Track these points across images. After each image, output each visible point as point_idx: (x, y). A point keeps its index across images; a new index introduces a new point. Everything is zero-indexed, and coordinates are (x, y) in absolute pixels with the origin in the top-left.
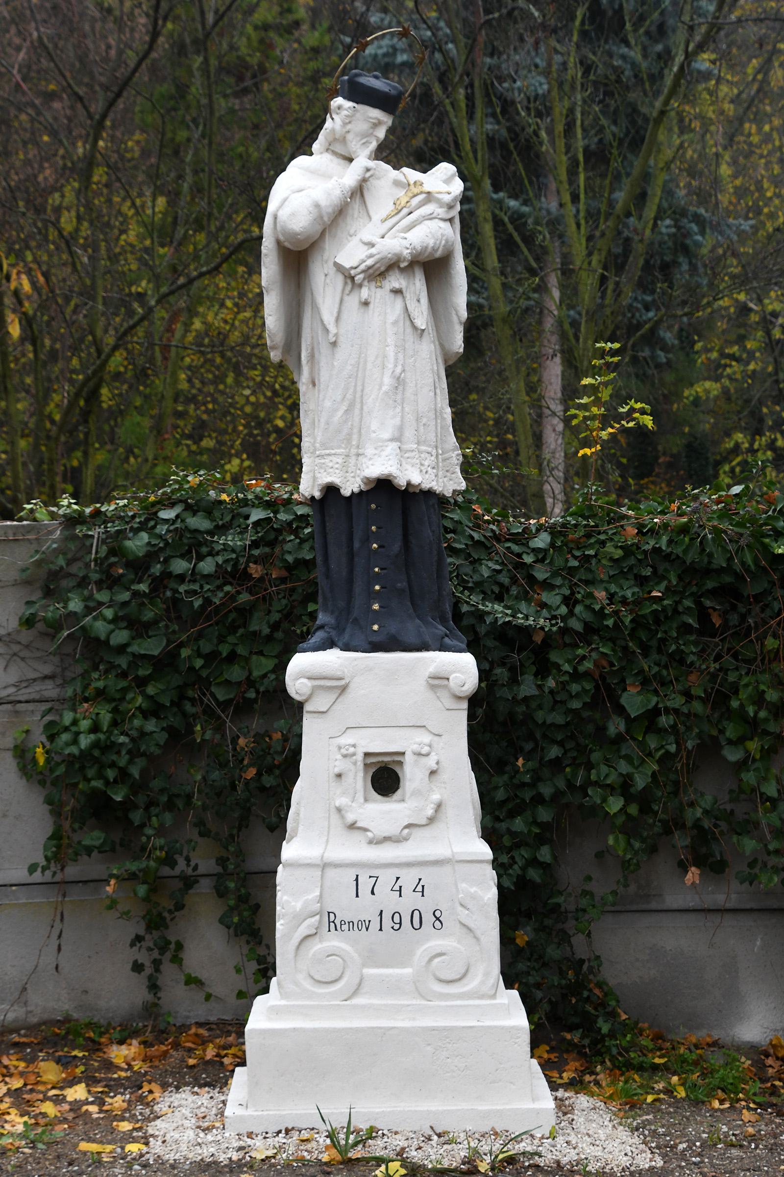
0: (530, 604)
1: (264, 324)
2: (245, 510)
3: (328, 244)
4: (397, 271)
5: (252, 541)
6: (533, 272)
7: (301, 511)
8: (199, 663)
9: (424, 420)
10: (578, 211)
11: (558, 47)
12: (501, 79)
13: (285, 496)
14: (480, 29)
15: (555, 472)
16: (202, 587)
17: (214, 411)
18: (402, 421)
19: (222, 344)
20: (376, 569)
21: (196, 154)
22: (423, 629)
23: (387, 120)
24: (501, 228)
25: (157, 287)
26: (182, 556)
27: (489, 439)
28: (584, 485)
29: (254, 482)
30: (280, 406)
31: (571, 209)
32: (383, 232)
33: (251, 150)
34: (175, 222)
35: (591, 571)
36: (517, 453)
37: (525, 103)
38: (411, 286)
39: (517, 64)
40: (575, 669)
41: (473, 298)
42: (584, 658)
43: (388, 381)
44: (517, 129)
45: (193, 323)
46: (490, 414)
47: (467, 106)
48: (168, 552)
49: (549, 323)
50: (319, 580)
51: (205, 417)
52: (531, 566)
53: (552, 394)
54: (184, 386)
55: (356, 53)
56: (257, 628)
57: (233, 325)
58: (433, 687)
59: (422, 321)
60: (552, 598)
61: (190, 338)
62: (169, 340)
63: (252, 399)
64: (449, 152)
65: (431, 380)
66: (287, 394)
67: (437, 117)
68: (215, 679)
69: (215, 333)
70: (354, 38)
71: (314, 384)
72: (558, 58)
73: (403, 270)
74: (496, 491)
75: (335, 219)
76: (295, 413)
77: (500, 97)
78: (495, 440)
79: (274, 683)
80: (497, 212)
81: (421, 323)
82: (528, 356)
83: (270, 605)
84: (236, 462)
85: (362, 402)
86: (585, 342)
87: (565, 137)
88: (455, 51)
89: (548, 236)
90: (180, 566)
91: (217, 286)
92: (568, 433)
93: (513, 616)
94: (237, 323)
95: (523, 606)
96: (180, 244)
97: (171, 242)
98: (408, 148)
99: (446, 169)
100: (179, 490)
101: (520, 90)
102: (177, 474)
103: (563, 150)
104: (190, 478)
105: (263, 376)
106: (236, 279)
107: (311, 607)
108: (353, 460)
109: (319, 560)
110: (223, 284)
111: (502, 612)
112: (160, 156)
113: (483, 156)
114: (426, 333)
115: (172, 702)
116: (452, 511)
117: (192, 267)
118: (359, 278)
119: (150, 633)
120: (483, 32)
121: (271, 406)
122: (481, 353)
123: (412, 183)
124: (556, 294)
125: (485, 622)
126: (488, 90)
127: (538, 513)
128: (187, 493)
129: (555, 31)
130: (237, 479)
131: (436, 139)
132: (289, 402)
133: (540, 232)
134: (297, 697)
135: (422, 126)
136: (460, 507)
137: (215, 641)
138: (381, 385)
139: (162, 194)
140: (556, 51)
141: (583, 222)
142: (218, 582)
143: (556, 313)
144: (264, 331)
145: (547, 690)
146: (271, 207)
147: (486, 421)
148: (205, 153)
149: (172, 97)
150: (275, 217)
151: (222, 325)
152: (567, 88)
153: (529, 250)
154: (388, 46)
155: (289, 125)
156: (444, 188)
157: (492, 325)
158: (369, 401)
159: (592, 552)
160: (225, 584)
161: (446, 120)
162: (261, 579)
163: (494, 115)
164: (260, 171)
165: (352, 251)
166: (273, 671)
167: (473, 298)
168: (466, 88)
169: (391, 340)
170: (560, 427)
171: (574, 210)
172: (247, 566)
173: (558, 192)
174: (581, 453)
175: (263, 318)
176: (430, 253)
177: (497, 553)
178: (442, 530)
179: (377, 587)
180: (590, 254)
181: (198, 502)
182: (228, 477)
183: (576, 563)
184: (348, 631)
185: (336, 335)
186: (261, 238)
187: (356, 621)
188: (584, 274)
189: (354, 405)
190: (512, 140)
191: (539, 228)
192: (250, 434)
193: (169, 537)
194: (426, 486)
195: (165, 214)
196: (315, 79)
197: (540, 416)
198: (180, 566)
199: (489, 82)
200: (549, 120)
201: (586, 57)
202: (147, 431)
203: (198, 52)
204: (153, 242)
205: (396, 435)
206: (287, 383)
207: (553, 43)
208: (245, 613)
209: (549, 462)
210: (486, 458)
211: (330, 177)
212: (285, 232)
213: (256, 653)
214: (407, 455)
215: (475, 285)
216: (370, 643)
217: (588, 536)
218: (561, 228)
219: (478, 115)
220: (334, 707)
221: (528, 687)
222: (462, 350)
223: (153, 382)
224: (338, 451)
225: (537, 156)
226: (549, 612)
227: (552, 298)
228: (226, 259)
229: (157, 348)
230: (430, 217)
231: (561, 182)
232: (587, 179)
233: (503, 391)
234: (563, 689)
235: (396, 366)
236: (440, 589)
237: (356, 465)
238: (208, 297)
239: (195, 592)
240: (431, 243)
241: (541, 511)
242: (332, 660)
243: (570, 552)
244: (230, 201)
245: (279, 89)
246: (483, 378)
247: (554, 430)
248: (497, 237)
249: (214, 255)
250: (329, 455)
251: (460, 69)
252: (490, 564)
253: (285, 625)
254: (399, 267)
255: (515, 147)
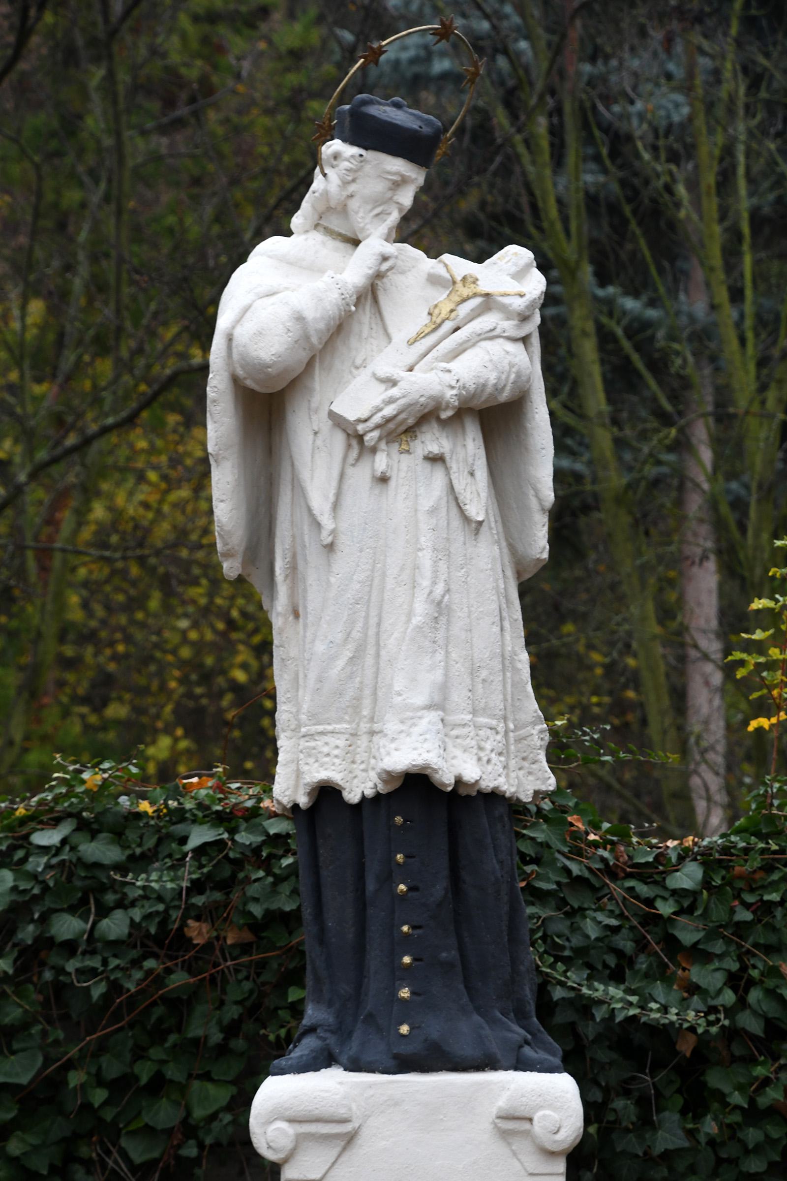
0: (670, 986)
1: (211, 512)
2: (179, 829)
3: (319, 381)
4: (435, 425)
5: (193, 881)
6: (666, 420)
7: (275, 827)
8: (99, 1096)
9: (484, 674)
10: (742, 316)
11: (706, 45)
12: (608, 99)
13: (250, 804)
14: (573, 18)
15: (711, 756)
16: (105, 962)
17: (126, 656)
18: (446, 675)
19: (141, 545)
20: (405, 928)
21: (95, 228)
22: (487, 1031)
23: (417, 176)
24: (610, 346)
25: (30, 452)
26: (72, 910)
27: (594, 699)
28: (759, 780)
29: (195, 780)
30: (241, 647)
31: (730, 313)
32: (410, 360)
33: (189, 221)
34: (60, 342)
35: (774, 929)
36: (644, 722)
37: (650, 137)
38: (459, 449)
39: (635, 74)
40: (752, 1102)
41: (565, 463)
42: (766, 1082)
43: (421, 609)
44: (636, 181)
45: (90, 510)
46: (596, 657)
47: (552, 145)
48: (48, 903)
49: (695, 504)
50: (306, 948)
51: (112, 667)
52: (670, 920)
53: (702, 623)
54: (76, 615)
55: (363, 68)
56: (200, 1032)
57: (159, 512)
58: (505, 1135)
59: (477, 510)
60: (708, 977)
61: (87, 534)
62: (51, 539)
63: (193, 635)
64: (522, 221)
65: (494, 606)
66: (251, 626)
67: (502, 164)
68: (126, 1126)
69: (129, 527)
70: (363, 37)
71: (296, 615)
72: (704, 62)
73: (444, 424)
74: (609, 788)
75: (329, 341)
76: (265, 658)
77: (606, 129)
78: (606, 699)
79: (230, 1129)
80: (604, 320)
81: (477, 510)
82: (660, 559)
83: (224, 991)
84: (165, 742)
85: (378, 644)
86: (757, 536)
87: (719, 193)
88: (530, 53)
89: (690, 359)
90: (68, 926)
91: (131, 446)
92: (729, 686)
93: (643, 1008)
94: (166, 508)
95: (658, 989)
96: (69, 378)
97: (54, 376)
98: (455, 222)
99: (515, 256)
100: (66, 796)
101: (641, 116)
102: (62, 768)
103: (715, 215)
104: (86, 776)
105: (211, 595)
106: (162, 436)
107: (294, 994)
108: (363, 742)
109: (307, 914)
110: (142, 444)
111: (621, 1000)
112: (34, 234)
113: (579, 227)
114: (484, 528)
115: (53, 1169)
116: (534, 826)
117: (90, 416)
118: (371, 438)
119: (16, 1046)
120: (578, 23)
121: (224, 647)
122: (580, 555)
123: (459, 278)
124: (706, 455)
125: (593, 1017)
126: (587, 119)
127: (681, 825)
128: (82, 801)
129: (699, 19)
130: (166, 774)
131: (500, 200)
132: (257, 639)
133: (678, 353)
134: (270, 1155)
135: (476, 179)
136: (546, 820)
137: (128, 1057)
138: (410, 615)
139: (37, 294)
140: (702, 52)
141: (750, 335)
142: (134, 954)
143: (706, 486)
144: (211, 522)
145: (703, 1139)
146: (223, 322)
147: (590, 668)
148: (110, 227)
149: (53, 134)
150: (230, 339)
151: (141, 511)
152: (720, 111)
153: (660, 383)
154: (418, 46)
155: (254, 178)
156: (513, 286)
157: (598, 509)
158: (391, 643)
159: (775, 897)
160: (145, 957)
161: (517, 169)
162: (208, 947)
163: (597, 158)
164: (203, 257)
165: (358, 393)
166: (228, 1108)
167: (565, 463)
168: (550, 115)
169: (426, 540)
170: (717, 678)
171: (735, 314)
172: (183, 924)
173: (708, 285)
174: (753, 725)
175: (210, 500)
176: (491, 394)
177: (612, 898)
178: (517, 859)
179: (407, 960)
180: (763, 388)
181: (98, 816)
182: (151, 768)
183: (745, 916)
184: (357, 1035)
185: (333, 532)
186: (205, 369)
187: (370, 1018)
188: (752, 422)
189: (365, 649)
190: (629, 200)
191: (676, 346)
192: (190, 695)
193: (50, 878)
194: (488, 784)
195: (43, 328)
196: (295, 102)
197: (682, 659)
198: (68, 926)
199: (588, 105)
200: (690, 166)
201: (754, 62)
202: (12, 692)
203: (96, 60)
204: (22, 377)
205: (437, 699)
206: (251, 609)
207: (697, 39)
208: (179, 1006)
209: (699, 738)
210: (589, 735)
211: (322, 271)
212: (243, 357)
213: (199, 1077)
214: (455, 732)
215: (569, 441)
216: (396, 1057)
217: (768, 868)
218: (712, 345)
219: (571, 159)
220: (332, 1173)
221: (669, 1135)
222: (545, 555)
223: (23, 609)
224: (338, 727)
225: (672, 225)
226: (704, 1001)
227: (700, 462)
228: (147, 403)
229: (30, 554)
230: (490, 335)
231: (712, 269)
232: (757, 263)
233: (618, 618)
234: (733, 1137)
235: (434, 583)
236: (514, 962)
237: (369, 750)
238: (116, 468)
239: (92, 972)
240: (492, 377)
241: (688, 824)
242: (328, 1087)
243: (737, 896)
244: (153, 306)
245: (235, 119)
246: (584, 596)
247: (707, 683)
248: (602, 363)
249: (127, 397)
250: (322, 733)
251: (539, 85)
252: (600, 916)
253: (249, 1027)
254: (438, 419)
255: (635, 212)
